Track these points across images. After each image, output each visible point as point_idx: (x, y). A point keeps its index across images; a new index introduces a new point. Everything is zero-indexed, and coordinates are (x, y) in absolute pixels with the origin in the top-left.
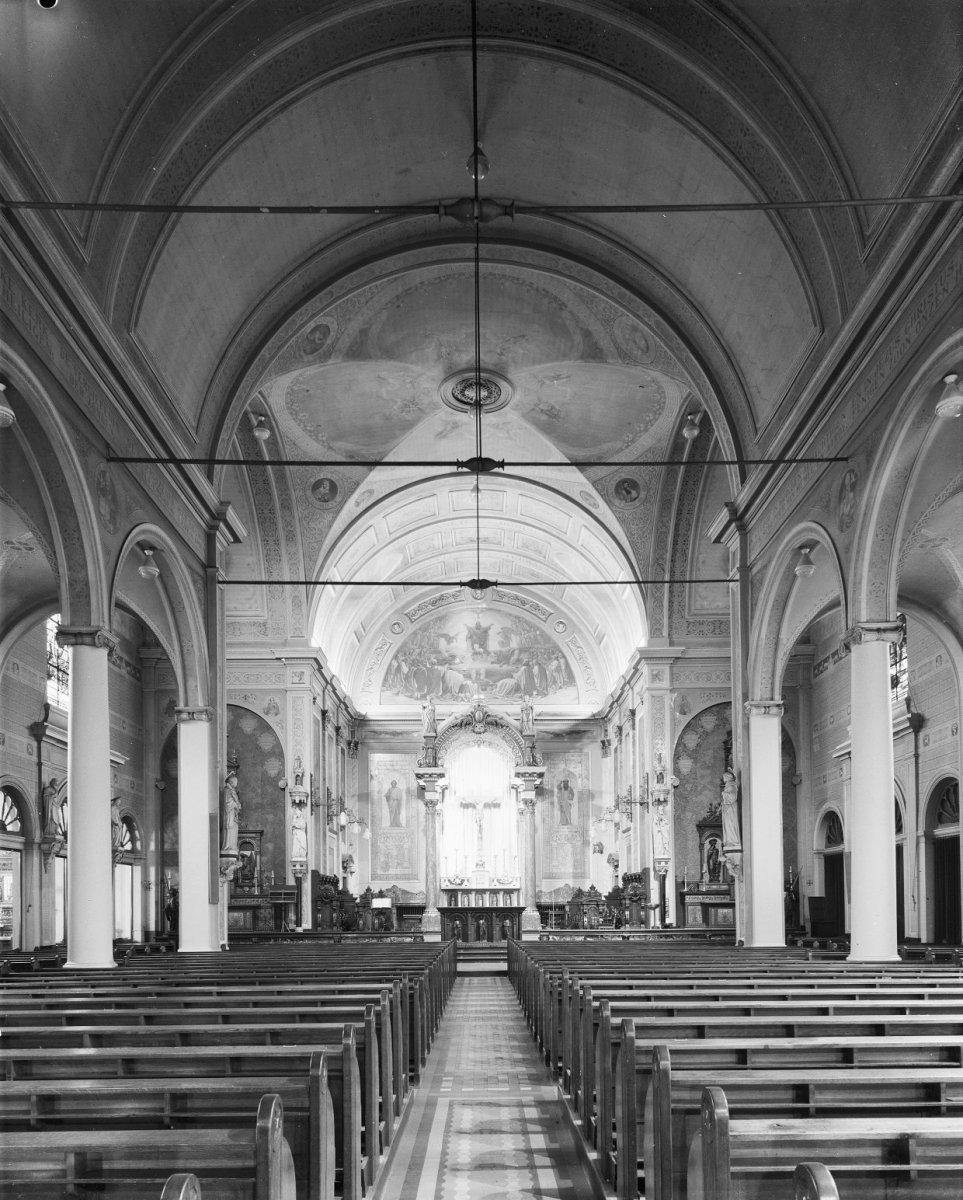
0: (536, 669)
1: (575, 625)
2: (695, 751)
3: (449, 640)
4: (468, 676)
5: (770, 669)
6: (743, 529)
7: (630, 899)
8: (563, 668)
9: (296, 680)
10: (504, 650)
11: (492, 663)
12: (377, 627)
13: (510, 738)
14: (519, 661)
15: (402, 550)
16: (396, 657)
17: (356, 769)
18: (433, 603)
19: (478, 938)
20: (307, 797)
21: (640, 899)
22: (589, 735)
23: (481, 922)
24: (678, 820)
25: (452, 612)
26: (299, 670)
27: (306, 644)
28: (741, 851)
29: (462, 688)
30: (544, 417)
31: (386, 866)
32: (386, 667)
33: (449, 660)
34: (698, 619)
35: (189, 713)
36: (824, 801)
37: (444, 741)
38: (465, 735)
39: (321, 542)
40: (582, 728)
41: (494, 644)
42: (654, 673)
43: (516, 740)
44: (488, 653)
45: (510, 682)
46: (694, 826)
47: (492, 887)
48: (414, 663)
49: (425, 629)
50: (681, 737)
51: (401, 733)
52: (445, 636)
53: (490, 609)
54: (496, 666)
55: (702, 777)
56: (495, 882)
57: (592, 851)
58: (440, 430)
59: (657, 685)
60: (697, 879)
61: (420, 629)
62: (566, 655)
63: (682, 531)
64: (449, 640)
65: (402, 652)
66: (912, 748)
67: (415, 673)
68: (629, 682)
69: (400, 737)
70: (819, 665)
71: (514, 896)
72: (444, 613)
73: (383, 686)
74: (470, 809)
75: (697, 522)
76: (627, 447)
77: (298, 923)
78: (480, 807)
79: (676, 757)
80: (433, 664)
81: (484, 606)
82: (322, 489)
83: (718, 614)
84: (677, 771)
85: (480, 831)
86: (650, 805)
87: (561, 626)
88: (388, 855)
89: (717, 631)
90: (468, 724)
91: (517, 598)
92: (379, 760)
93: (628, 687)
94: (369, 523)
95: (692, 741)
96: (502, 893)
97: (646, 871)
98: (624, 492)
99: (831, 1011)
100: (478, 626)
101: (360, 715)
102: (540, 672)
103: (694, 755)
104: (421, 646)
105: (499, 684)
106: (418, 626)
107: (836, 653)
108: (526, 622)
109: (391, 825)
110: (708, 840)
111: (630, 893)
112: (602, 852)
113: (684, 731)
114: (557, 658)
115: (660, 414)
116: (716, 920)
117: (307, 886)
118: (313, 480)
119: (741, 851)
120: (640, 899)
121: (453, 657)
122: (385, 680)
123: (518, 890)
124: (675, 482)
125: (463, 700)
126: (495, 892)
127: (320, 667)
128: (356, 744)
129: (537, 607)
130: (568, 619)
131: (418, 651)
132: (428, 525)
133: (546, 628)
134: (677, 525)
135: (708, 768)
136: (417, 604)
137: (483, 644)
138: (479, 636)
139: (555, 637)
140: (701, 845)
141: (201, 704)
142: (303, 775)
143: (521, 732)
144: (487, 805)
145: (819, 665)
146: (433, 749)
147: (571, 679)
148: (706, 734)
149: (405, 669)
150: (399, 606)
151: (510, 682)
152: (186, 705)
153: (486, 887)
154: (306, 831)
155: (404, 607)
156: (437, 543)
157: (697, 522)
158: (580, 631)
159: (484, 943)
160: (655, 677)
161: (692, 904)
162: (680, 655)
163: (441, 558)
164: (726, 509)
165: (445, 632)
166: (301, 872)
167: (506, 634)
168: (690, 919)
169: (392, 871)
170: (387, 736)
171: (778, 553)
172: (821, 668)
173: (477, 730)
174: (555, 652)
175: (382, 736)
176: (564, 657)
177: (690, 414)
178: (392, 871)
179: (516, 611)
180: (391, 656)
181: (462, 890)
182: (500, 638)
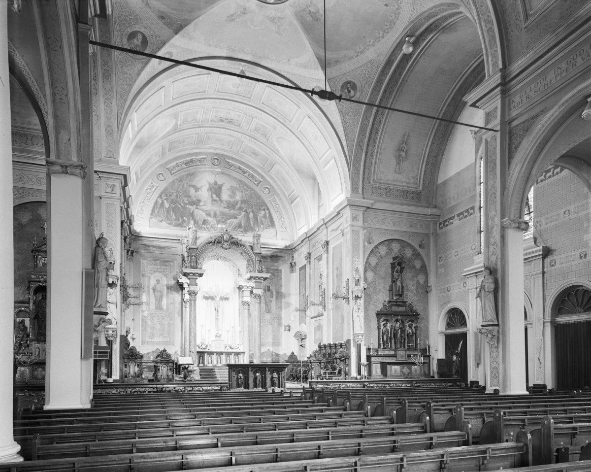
0: (251, 215)
1: (275, 190)
2: (375, 268)
3: (197, 189)
4: (209, 215)
5: (521, 196)
6: (505, 93)
7: (340, 359)
8: (268, 215)
9: (109, 190)
10: (232, 200)
11: (224, 208)
12: (147, 175)
13: (245, 254)
14: (240, 208)
15: (176, 116)
16: (160, 196)
17: (132, 269)
18: (186, 164)
19: (255, 386)
20: (118, 279)
21: (345, 359)
22: (283, 259)
23: (258, 374)
24: (366, 309)
25: (200, 172)
26: (112, 183)
27: (117, 163)
28: (498, 325)
29: (205, 222)
30: (309, 19)
31: (152, 335)
32: (153, 202)
33: (197, 203)
34: (379, 185)
35: (62, 166)
36: (448, 302)
37: (202, 252)
38: (217, 250)
39: (131, 86)
40: (279, 254)
41: (225, 196)
42: (354, 216)
43: (250, 256)
44: (222, 201)
45: (235, 221)
46: (375, 315)
47: (226, 351)
48: (173, 202)
49: (181, 180)
50: (368, 258)
51: (164, 248)
52: (194, 186)
53: (223, 173)
54: (227, 210)
55: (379, 284)
56: (228, 348)
57: (283, 330)
58: (232, 13)
59: (355, 223)
60: (376, 347)
61: (177, 179)
62: (270, 208)
63: (375, 126)
64: (197, 189)
65: (165, 194)
66: (541, 268)
67: (174, 208)
68: (326, 224)
69: (163, 250)
70: (445, 221)
71: (241, 357)
72: (193, 171)
73: (152, 214)
74: (210, 300)
75: (385, 121)
76: (356, 57)
77: (109, 375)
78: (218, 299)
79: (365, 271)
80: (186, 204)
81: (219, 170)
82: (135, 40)
83: (389, 184)
84: (365, 279)
85: (217, 314)
86: (351, 299)
87: (267, 189)
88: (153, 328)
89: (388, 194)
90: (219, 242)
91: (240, 168)
92: (147, 265)
93: (324, 226)
94: (161, 85)
95: (374, 261)
96: (233, 354)
97: (348, 341)
98: (346, 91)
99: (300, 411)
100: (215, 183)
101: (136, 233)
102: (254, 217)
103: (375, 269)
104: (177, 191)
105: (229, 221)
106: (176, 178)
107: (462, 213)
108: (246, 185)
109: (156, 308)
110: (408, 324)
111: (332, 357)
112: (289, 330)
113: (370, 255)
114: (264, 210)
115: (387, 33)
116: (391, 372)
117: (116, 347)
118: (130, 30)
119: (498, 325)
120: (345, 359)
121: (199, 201)
122: (153, 211)
123: (244, 353)
124: (380, 89)
125: (205, 229)
126: (228, 354)
127: (126, 184)
128: (132, 253)
129: (252, 176)
130: (271, 185)
131: (175, 194)
132: (199, 99)
133: (257, 189)
134: (374, 121)
135: (382, 278)
136: (175, 163)
137: (219, 195)
138: (216, 190)
139: (263, 196)
140: (379, 326)
141: (75, 159)
142: (114, 263)
143: (252, 249)
144: (221, 299)
145: (445, 221)
146: (194, 257)
147: (272, 224)
148: (381, 257)
149: (167, 205)
150: (164, 161)
151: (235, 221)
152: (58, 157)
153: (222, 350)
154: (116, 305)
155: (166, 163)
156: (199, 117)
157: (385, 121)
158: (278, 195)
159: (242, 389)
160: (354, 218)
161: (376, 363)
162: (370, 206)
163: (198, 130)
164: (500, 74)
165: (194, 183)
166: (112, 337)
167: (233, 190)
168: (374, 373)
169: (156, 339)
170: (154, 249)
171: (562, 101)
172: (447, 223)
173: (224, 246)
174: (263, 206)
175: (151, 248)
176: (268, 209)
177: (408, 36)
178: (156, 339)
179: (239, 177)
180: (157, 195)
181: (206, 352)
182: (229, 193)
